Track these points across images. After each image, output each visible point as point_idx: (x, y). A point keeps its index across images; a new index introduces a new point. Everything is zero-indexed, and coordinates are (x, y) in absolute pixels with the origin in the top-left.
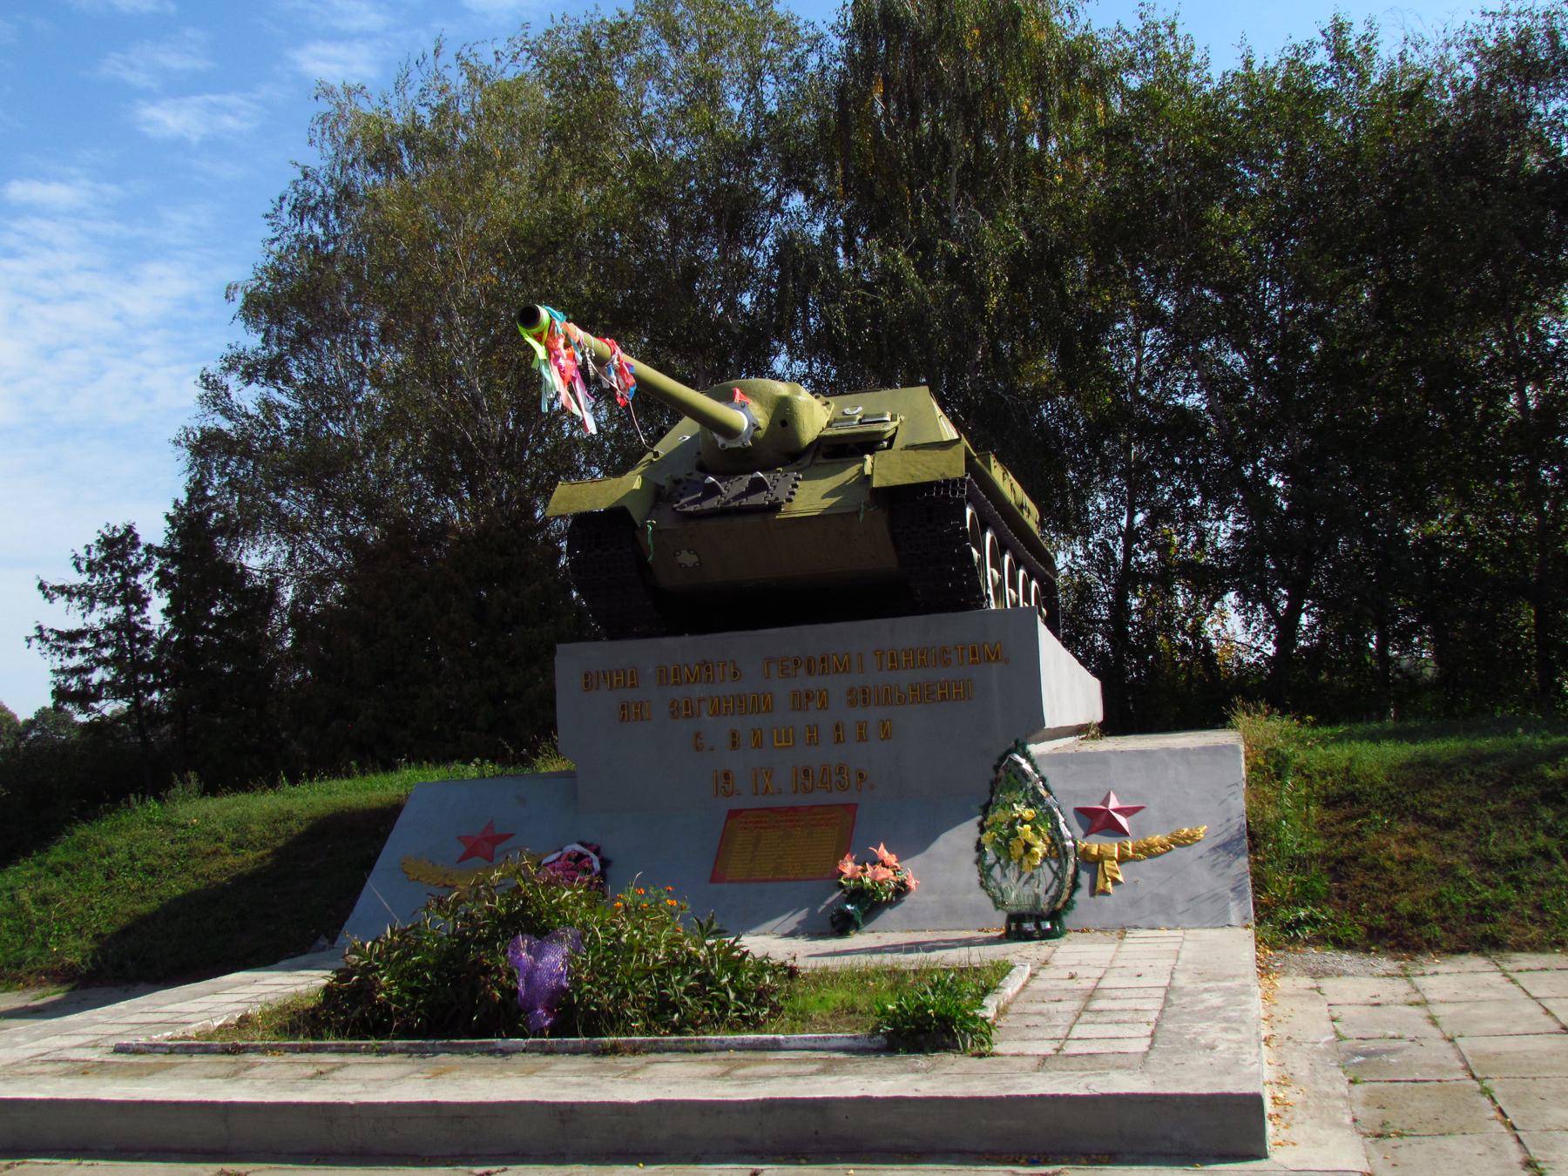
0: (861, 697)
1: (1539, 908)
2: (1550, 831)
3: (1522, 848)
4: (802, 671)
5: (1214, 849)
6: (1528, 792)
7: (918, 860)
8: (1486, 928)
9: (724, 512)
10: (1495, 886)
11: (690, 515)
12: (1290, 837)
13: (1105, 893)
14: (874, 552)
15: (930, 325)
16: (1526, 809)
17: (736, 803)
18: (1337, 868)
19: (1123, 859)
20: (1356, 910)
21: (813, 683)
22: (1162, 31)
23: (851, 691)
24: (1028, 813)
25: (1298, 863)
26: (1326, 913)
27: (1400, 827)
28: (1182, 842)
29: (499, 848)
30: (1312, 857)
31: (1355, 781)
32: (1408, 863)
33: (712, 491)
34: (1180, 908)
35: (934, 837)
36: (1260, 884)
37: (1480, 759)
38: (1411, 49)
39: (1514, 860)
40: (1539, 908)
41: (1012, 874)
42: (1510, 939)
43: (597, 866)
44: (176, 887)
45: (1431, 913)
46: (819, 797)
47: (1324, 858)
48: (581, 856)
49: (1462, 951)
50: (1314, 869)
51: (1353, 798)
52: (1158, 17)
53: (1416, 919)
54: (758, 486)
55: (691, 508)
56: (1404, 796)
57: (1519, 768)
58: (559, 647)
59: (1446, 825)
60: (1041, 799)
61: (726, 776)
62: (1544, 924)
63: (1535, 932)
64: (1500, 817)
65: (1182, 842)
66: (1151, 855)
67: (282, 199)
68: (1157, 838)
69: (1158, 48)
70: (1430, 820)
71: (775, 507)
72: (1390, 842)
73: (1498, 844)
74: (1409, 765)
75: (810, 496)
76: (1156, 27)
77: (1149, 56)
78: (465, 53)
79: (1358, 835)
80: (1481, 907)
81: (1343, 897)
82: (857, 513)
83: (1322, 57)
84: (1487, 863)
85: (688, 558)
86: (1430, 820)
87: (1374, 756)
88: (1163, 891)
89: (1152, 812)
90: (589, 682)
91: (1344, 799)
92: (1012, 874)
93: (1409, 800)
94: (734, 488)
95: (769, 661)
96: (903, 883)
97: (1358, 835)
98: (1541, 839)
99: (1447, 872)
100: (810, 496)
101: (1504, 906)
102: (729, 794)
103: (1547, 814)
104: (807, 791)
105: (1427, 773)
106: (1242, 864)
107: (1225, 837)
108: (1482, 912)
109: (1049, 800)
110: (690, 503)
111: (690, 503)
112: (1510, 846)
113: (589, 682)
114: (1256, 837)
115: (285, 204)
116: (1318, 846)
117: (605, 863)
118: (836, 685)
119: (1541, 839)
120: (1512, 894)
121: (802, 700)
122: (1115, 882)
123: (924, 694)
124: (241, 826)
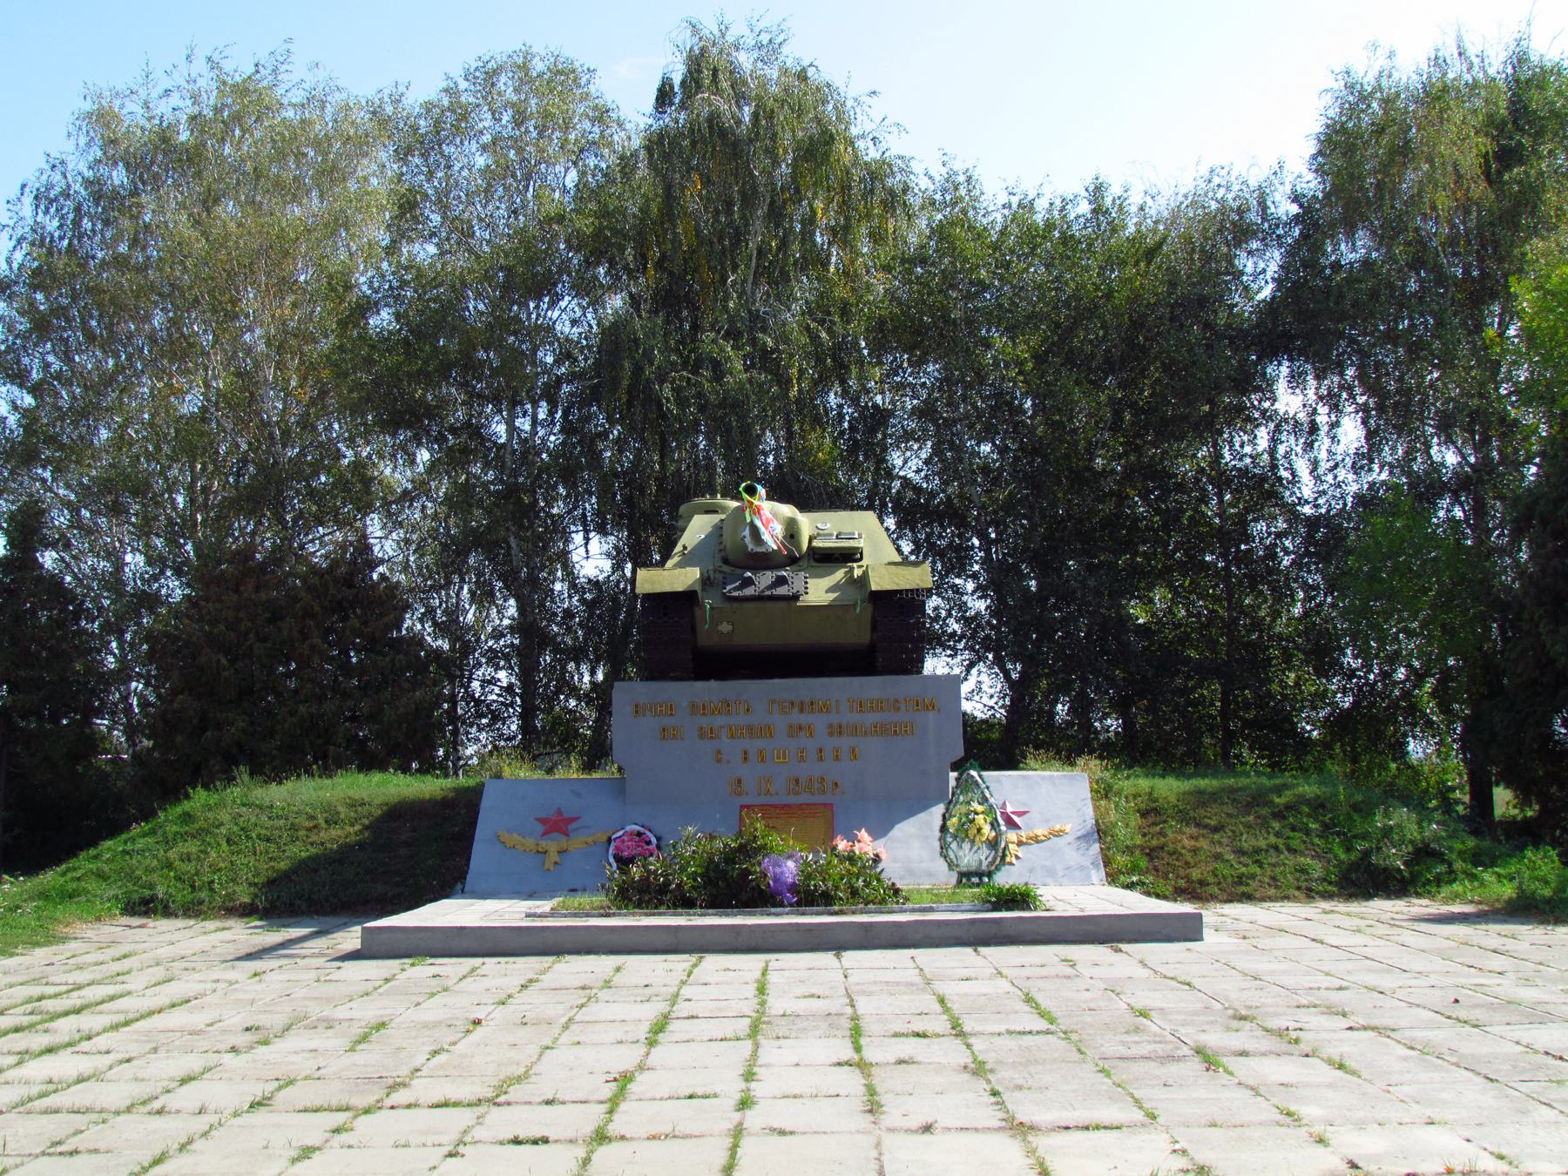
0: (837, 730)
1: (1273, 878)
2: (1278, 835)
3: (1262, 843)
4: (796, 709)
5: (1078, 838)
6: (1264, 811)
7: (883, 840)
8: (1243, 888)
9: (759, 598)
10: (1246, 865)
11: (736, 599)
12: (1121, 832)
13: (1011, 864)
14: (858, 633)
15: (749, 411)
16: (1264, 824)
17: (745, 800)
18: (1151, 853)
19: (1020, 844)
20: (1166, 877)
21: (805, 719)
22: (961, 179)
23: (831, 726)
24: (980, 808)
25: (1129, 850)
26: (1149, 879)
27: (1188, 830)
28: (1058, 834)
29: (570, 827)
30: (1135, 846)
31: (1156, 800)
32: (1195, 851)
33: (748, 582)
34: (1060, 873)
35: (891, 827)
36: (1107, 862)
37: (1232, 790)
38: (1148, 200)
39: (1257, 851)
40: (1273, 878)
41: (966, 846)
42: (1258, 895)
43: (654, 840)
44: (300, 851)
45: (1211, 880)
46: (804, 798)
47: (1142, 848)
48: (639, 834)
49: (1231, 901)
50: (1137, 852)
51: (1156, 811)
52: (958, 166)
53: (1202, 883)
54: (781, 581)
55: (736, 594)
56: (1190, 811)
57: (1257, 799)
58: (616, 684)
59: (1215, 830)
60: (986, 800)
61: (739, 781)
62: (1277, 887)
63: (1272, 892)
64: (1248, 826)
65: (1058, 834)
66: (1038, 842)
67: (24, 186)
68: (1040, 832)
69: (957, 194)
70: (1206, 826)
71: (796, 597)
72: (1182, 837)
73: (1247, 842)
74: (1190, 793)
75: (819, 590)
76: (956, 174)
77: (948, 198)
78: (216, 57)
79: (1162, 834)
80: (1240, 877)
81: (1156, 870)
82: (855, 606)
83: (1084, 208)
84: (1240, 852)
85: (725, 627)
86: (1206, 826)
87: (1169, 788)
88: (1048, 863)
89: (1035, 815)
90: (638, 710)
91: (1151, 812)
92: (966, 846)
93: (1192, 814)
94: (765, 579)
95: (773, 701)
96: (877, 855)
97: (1162, 834)
98: (1273, 839)
99: (1217, 857)
100: (819, 590)
101: (1253, 876)
102: (740, 794)
103: (1276, 825)
104: (797, 794)
105: (1203, 799)
106: (1096, 847)
107: (1083, 832)
108: (1240, 880)
109: (992, 800)
110: (735, 589)
111: (735, 589)
112: (1253, 842)
113: (638, 710)
114: (1101, 832)
115: (27, 190)
116: (1139, 840)
117: (658, 839)
118: (819, 722)
119: (1273, 839)
120: (1255, 869)
121: (795, 730)
122: (1017, 857)
123: (882, 730)
124: (353, 804)
